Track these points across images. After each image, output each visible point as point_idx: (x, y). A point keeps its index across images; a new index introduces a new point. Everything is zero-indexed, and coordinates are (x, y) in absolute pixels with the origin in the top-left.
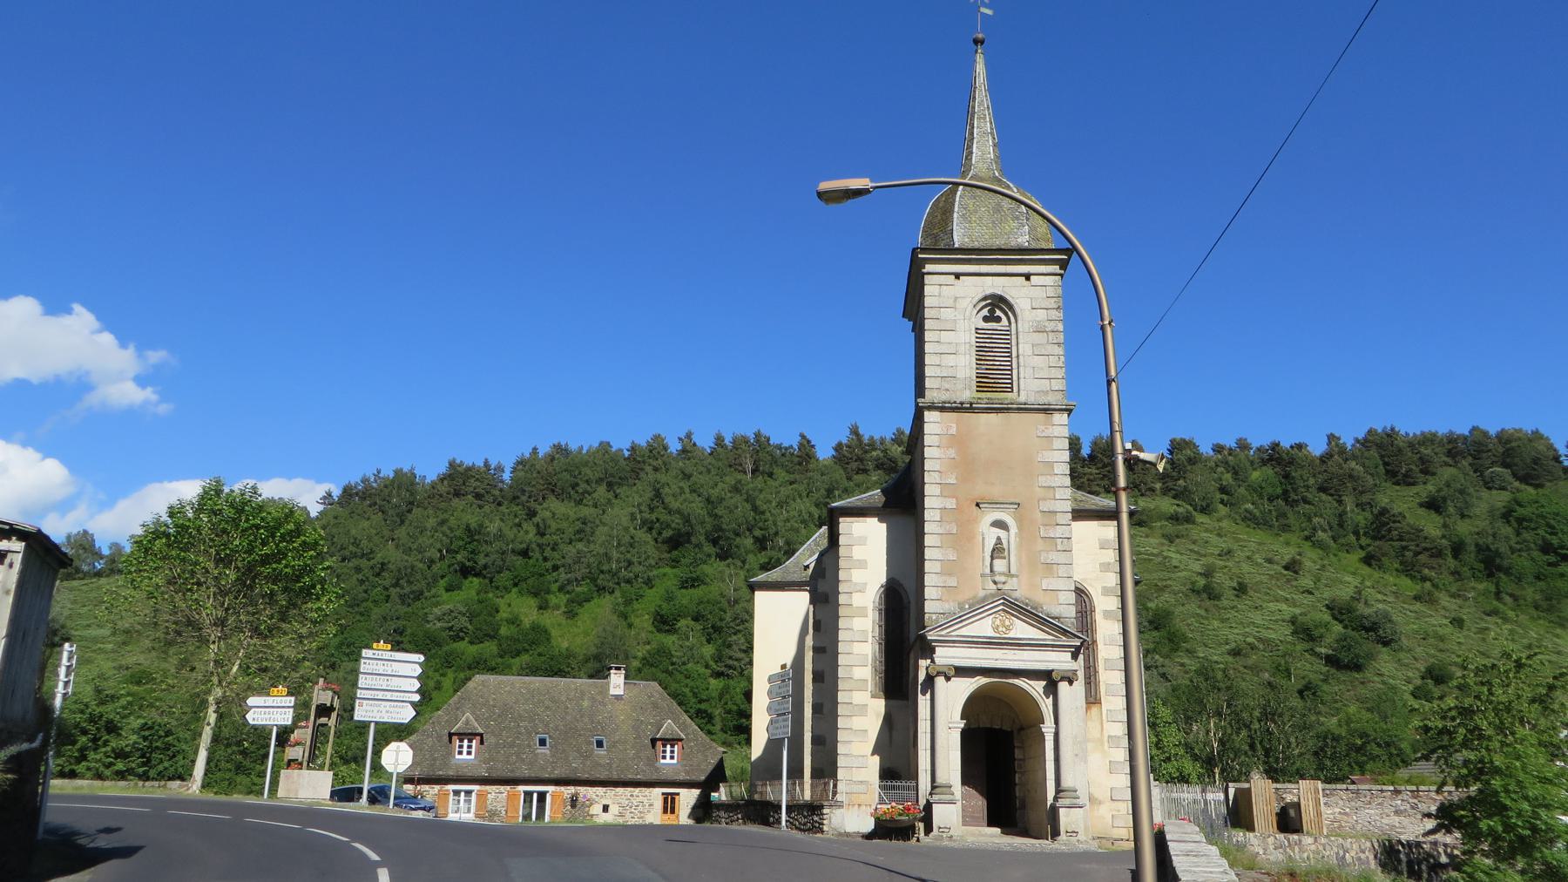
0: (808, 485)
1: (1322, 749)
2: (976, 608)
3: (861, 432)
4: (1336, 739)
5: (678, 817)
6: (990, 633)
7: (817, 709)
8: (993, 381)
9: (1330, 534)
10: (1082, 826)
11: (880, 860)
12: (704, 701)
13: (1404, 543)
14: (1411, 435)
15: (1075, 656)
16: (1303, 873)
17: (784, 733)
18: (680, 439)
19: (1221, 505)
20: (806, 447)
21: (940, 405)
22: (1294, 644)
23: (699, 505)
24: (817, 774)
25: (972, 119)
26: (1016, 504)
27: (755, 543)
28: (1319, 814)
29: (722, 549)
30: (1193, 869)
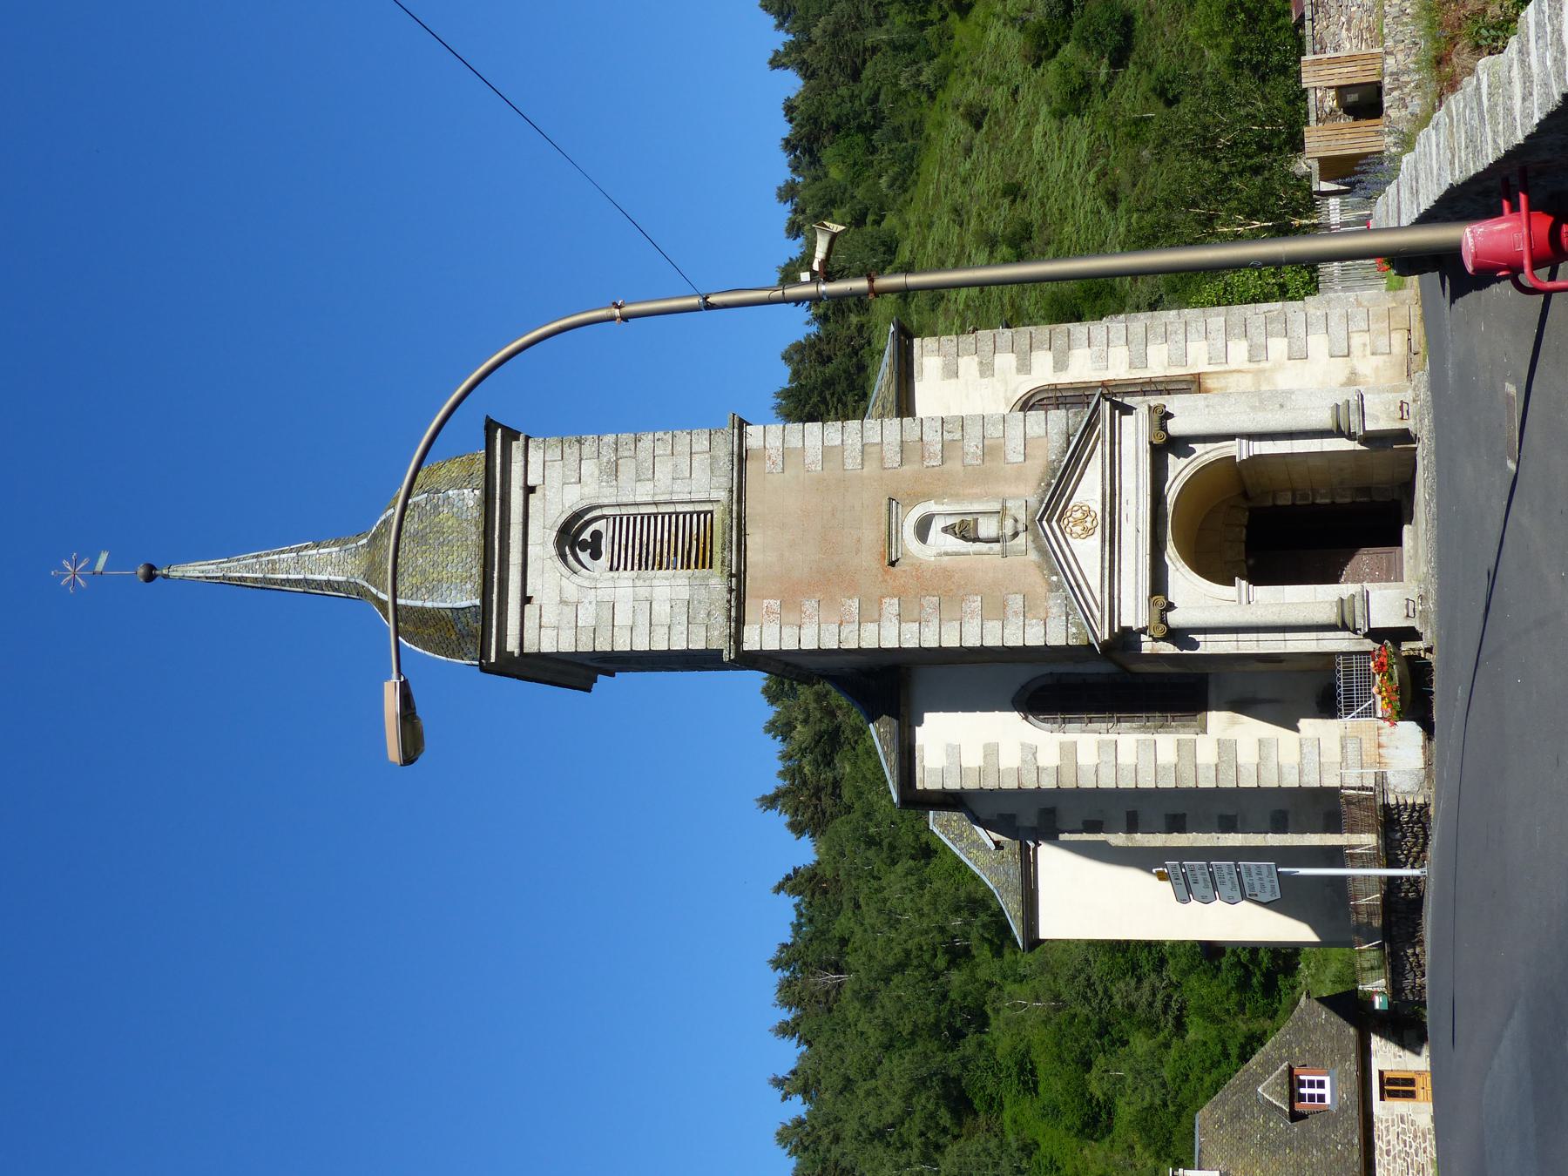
0: (859, 877)
1: (1255, 68)
2: (1055, 564)
3: (770, 791)
4: (1238, 49)
5: (1419, 1073)
6: (1096, 540)
7: (1228, 826)
8: (694, 543)
9: (924, 63)
10: (1391, 396)
11: (1462, 693)
12: (1225, 1048)
15: (1127, 410)
16: (1436, 46)
17: (1270, 873)
18: (785, 1098)
19: (884, 224)
20: (794, 883)
21: (733, 624)
22: (1095, 113)
23: (895, 1062)
24: (1334, 826)
25: (275, 582)
26: (890, 504)
27: (958, 967)
28: (1352, 59)
29: (969, 1023)
30: (1435, 172)
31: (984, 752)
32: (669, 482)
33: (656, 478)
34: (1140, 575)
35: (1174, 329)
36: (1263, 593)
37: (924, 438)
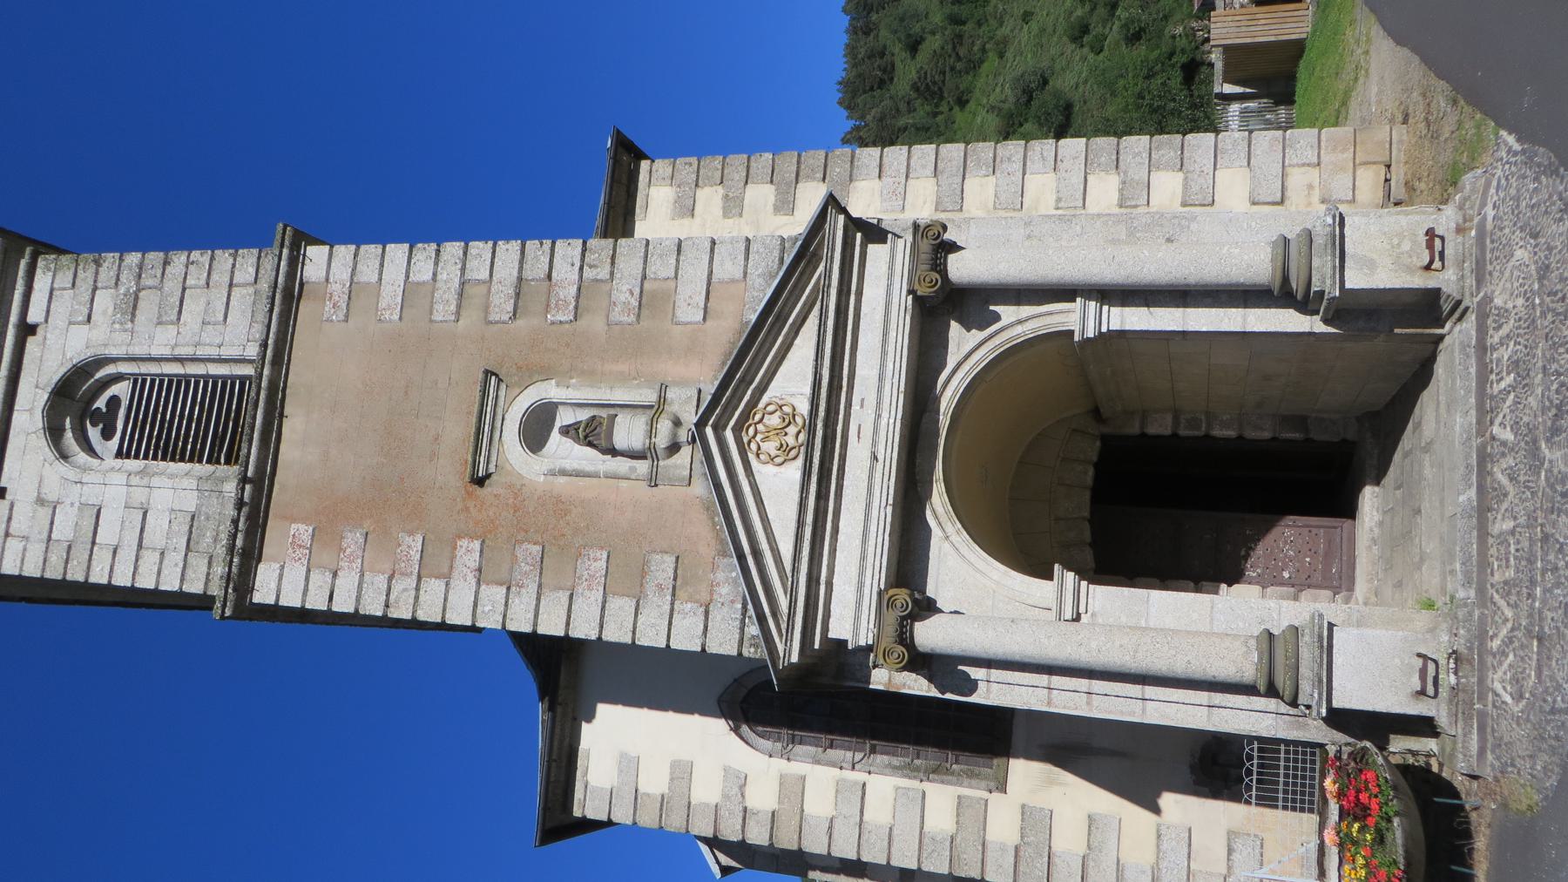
6: (794, 471)
13: (947, 69)
14: (846, 66)
26: (486, 383)
31: (671, 774)
32: (197, 327)
33: (182, 321)
34: (872, 542)
35: (1007, 154)
36: (1107, 600)
37: (554, 275)
